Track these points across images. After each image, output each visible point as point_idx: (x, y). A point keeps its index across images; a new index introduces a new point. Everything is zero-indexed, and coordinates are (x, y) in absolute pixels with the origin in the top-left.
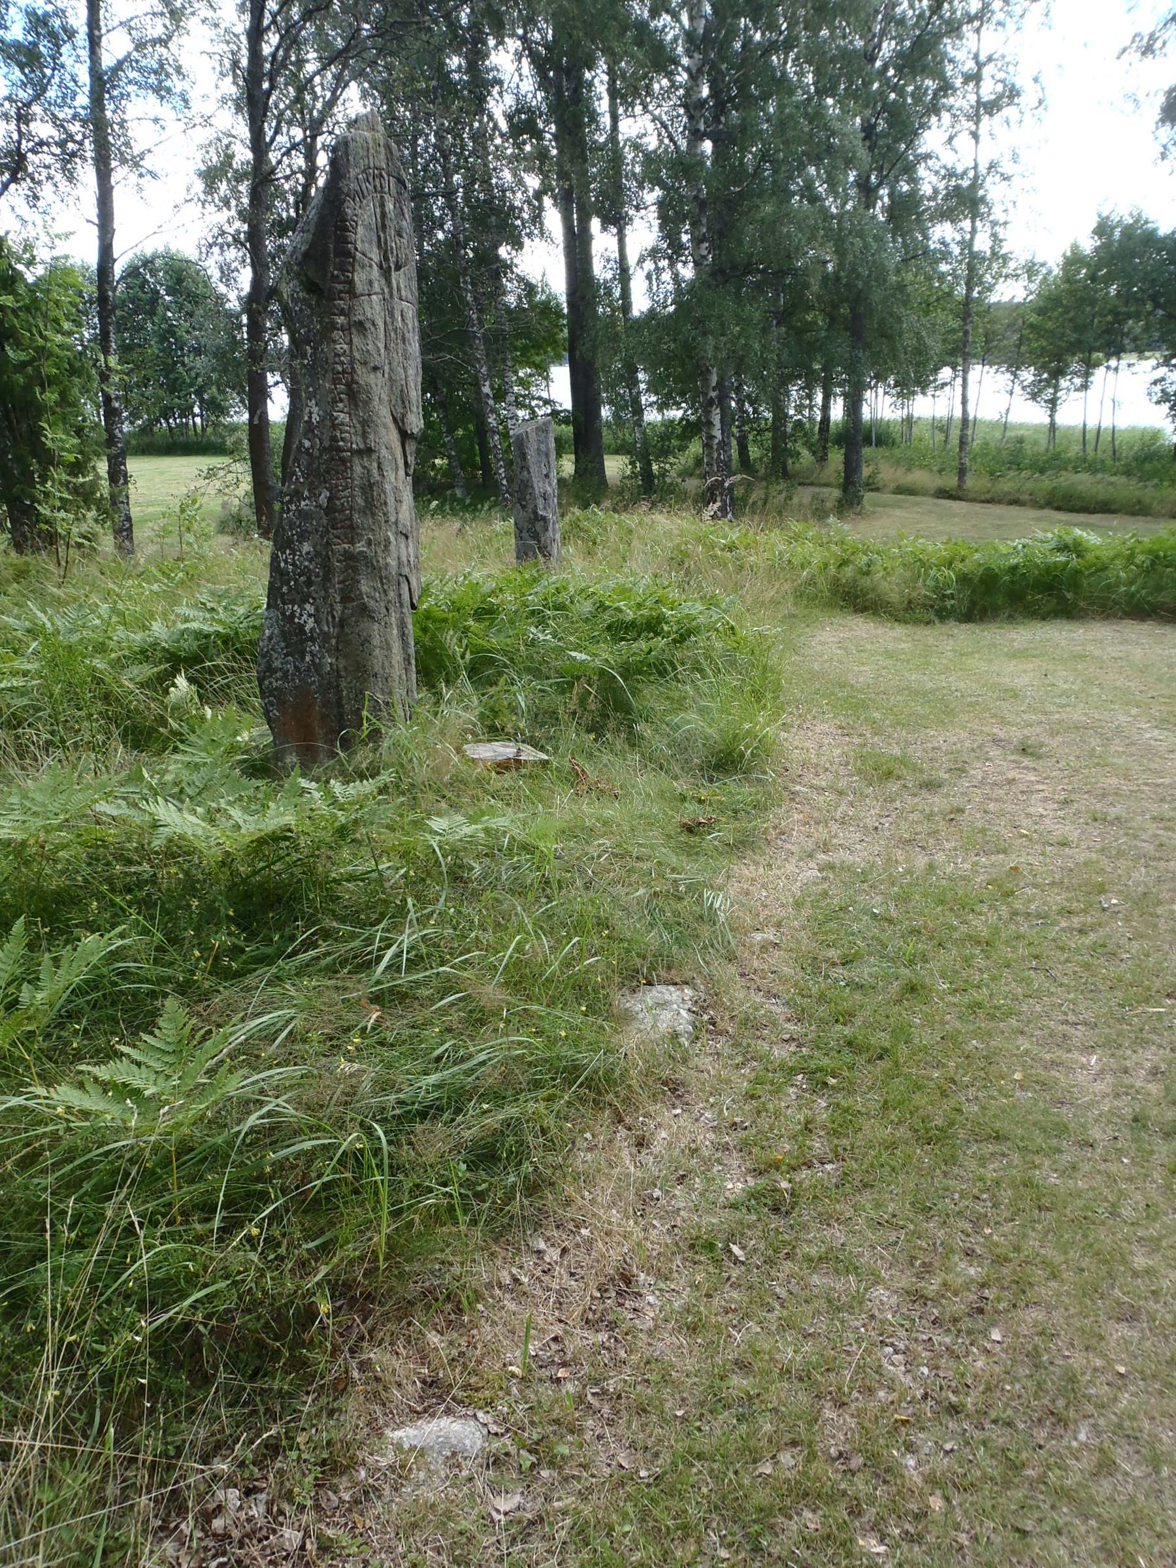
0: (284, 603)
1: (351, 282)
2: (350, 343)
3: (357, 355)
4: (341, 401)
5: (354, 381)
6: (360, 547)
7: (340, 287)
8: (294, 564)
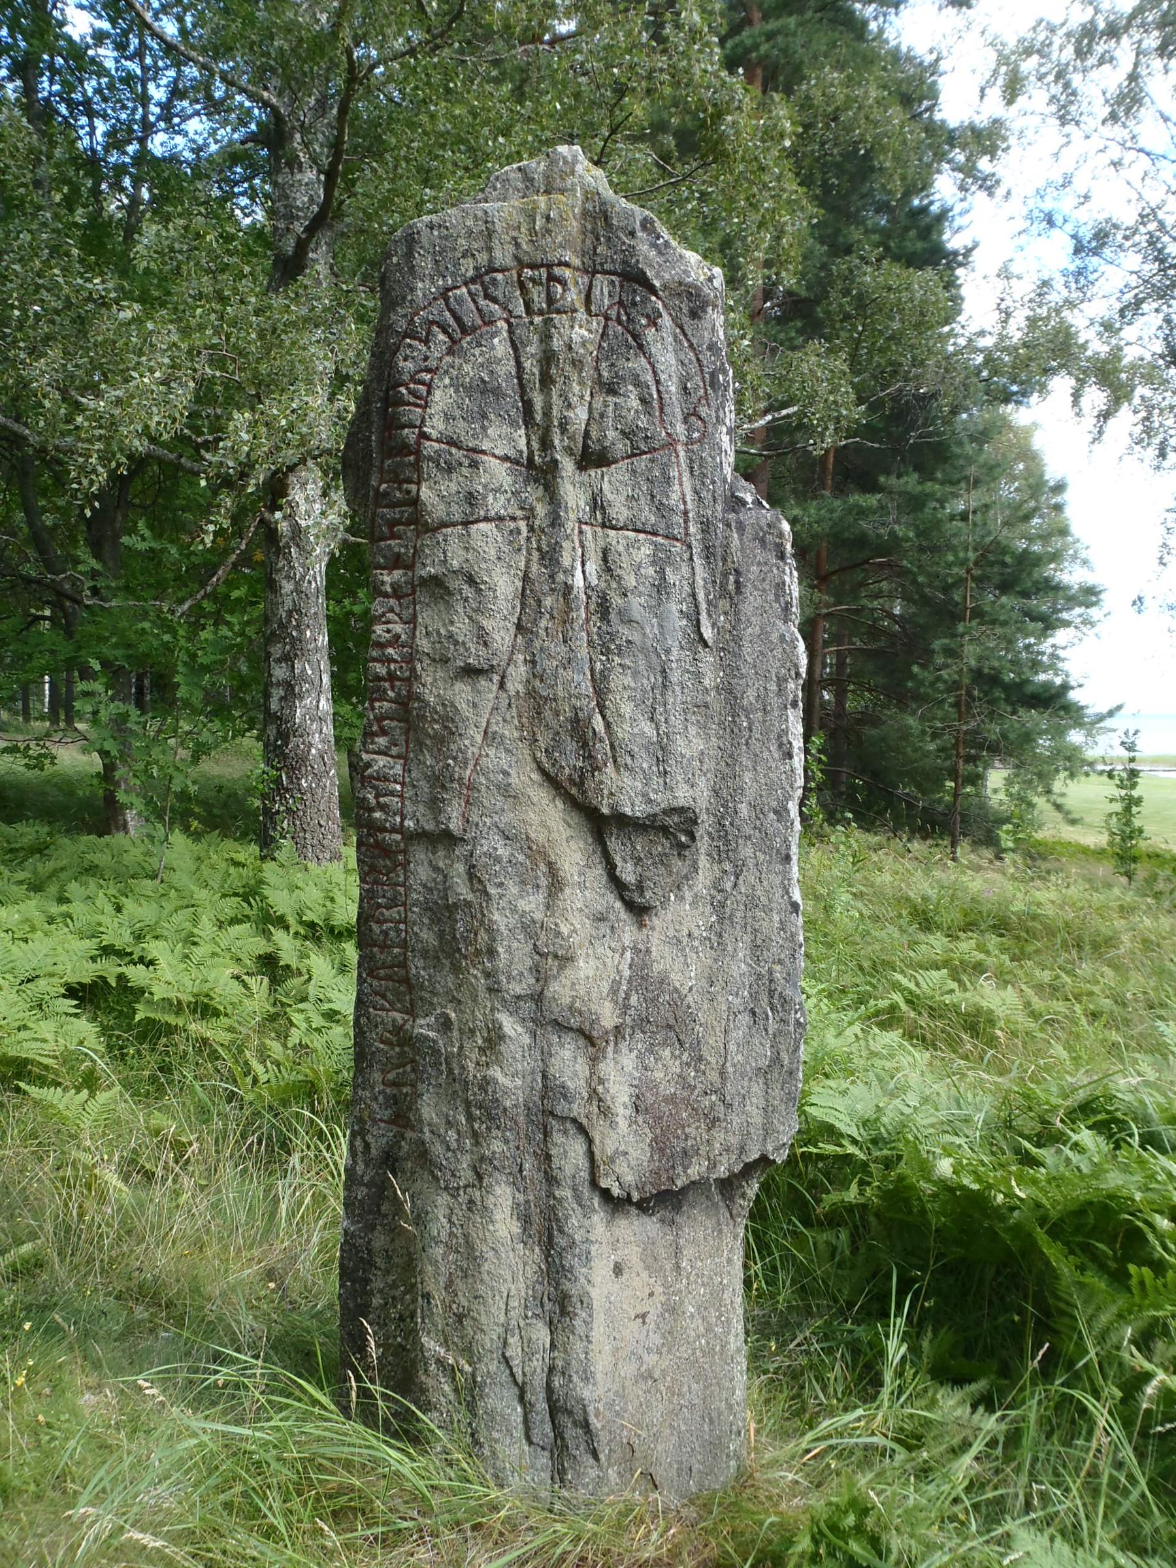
1: (415, 501)
2: (412, 621)
3: (424, 644)
4: (383, 732)
5: (412, 696)
6: (424, 1027)
7: (396, 513)
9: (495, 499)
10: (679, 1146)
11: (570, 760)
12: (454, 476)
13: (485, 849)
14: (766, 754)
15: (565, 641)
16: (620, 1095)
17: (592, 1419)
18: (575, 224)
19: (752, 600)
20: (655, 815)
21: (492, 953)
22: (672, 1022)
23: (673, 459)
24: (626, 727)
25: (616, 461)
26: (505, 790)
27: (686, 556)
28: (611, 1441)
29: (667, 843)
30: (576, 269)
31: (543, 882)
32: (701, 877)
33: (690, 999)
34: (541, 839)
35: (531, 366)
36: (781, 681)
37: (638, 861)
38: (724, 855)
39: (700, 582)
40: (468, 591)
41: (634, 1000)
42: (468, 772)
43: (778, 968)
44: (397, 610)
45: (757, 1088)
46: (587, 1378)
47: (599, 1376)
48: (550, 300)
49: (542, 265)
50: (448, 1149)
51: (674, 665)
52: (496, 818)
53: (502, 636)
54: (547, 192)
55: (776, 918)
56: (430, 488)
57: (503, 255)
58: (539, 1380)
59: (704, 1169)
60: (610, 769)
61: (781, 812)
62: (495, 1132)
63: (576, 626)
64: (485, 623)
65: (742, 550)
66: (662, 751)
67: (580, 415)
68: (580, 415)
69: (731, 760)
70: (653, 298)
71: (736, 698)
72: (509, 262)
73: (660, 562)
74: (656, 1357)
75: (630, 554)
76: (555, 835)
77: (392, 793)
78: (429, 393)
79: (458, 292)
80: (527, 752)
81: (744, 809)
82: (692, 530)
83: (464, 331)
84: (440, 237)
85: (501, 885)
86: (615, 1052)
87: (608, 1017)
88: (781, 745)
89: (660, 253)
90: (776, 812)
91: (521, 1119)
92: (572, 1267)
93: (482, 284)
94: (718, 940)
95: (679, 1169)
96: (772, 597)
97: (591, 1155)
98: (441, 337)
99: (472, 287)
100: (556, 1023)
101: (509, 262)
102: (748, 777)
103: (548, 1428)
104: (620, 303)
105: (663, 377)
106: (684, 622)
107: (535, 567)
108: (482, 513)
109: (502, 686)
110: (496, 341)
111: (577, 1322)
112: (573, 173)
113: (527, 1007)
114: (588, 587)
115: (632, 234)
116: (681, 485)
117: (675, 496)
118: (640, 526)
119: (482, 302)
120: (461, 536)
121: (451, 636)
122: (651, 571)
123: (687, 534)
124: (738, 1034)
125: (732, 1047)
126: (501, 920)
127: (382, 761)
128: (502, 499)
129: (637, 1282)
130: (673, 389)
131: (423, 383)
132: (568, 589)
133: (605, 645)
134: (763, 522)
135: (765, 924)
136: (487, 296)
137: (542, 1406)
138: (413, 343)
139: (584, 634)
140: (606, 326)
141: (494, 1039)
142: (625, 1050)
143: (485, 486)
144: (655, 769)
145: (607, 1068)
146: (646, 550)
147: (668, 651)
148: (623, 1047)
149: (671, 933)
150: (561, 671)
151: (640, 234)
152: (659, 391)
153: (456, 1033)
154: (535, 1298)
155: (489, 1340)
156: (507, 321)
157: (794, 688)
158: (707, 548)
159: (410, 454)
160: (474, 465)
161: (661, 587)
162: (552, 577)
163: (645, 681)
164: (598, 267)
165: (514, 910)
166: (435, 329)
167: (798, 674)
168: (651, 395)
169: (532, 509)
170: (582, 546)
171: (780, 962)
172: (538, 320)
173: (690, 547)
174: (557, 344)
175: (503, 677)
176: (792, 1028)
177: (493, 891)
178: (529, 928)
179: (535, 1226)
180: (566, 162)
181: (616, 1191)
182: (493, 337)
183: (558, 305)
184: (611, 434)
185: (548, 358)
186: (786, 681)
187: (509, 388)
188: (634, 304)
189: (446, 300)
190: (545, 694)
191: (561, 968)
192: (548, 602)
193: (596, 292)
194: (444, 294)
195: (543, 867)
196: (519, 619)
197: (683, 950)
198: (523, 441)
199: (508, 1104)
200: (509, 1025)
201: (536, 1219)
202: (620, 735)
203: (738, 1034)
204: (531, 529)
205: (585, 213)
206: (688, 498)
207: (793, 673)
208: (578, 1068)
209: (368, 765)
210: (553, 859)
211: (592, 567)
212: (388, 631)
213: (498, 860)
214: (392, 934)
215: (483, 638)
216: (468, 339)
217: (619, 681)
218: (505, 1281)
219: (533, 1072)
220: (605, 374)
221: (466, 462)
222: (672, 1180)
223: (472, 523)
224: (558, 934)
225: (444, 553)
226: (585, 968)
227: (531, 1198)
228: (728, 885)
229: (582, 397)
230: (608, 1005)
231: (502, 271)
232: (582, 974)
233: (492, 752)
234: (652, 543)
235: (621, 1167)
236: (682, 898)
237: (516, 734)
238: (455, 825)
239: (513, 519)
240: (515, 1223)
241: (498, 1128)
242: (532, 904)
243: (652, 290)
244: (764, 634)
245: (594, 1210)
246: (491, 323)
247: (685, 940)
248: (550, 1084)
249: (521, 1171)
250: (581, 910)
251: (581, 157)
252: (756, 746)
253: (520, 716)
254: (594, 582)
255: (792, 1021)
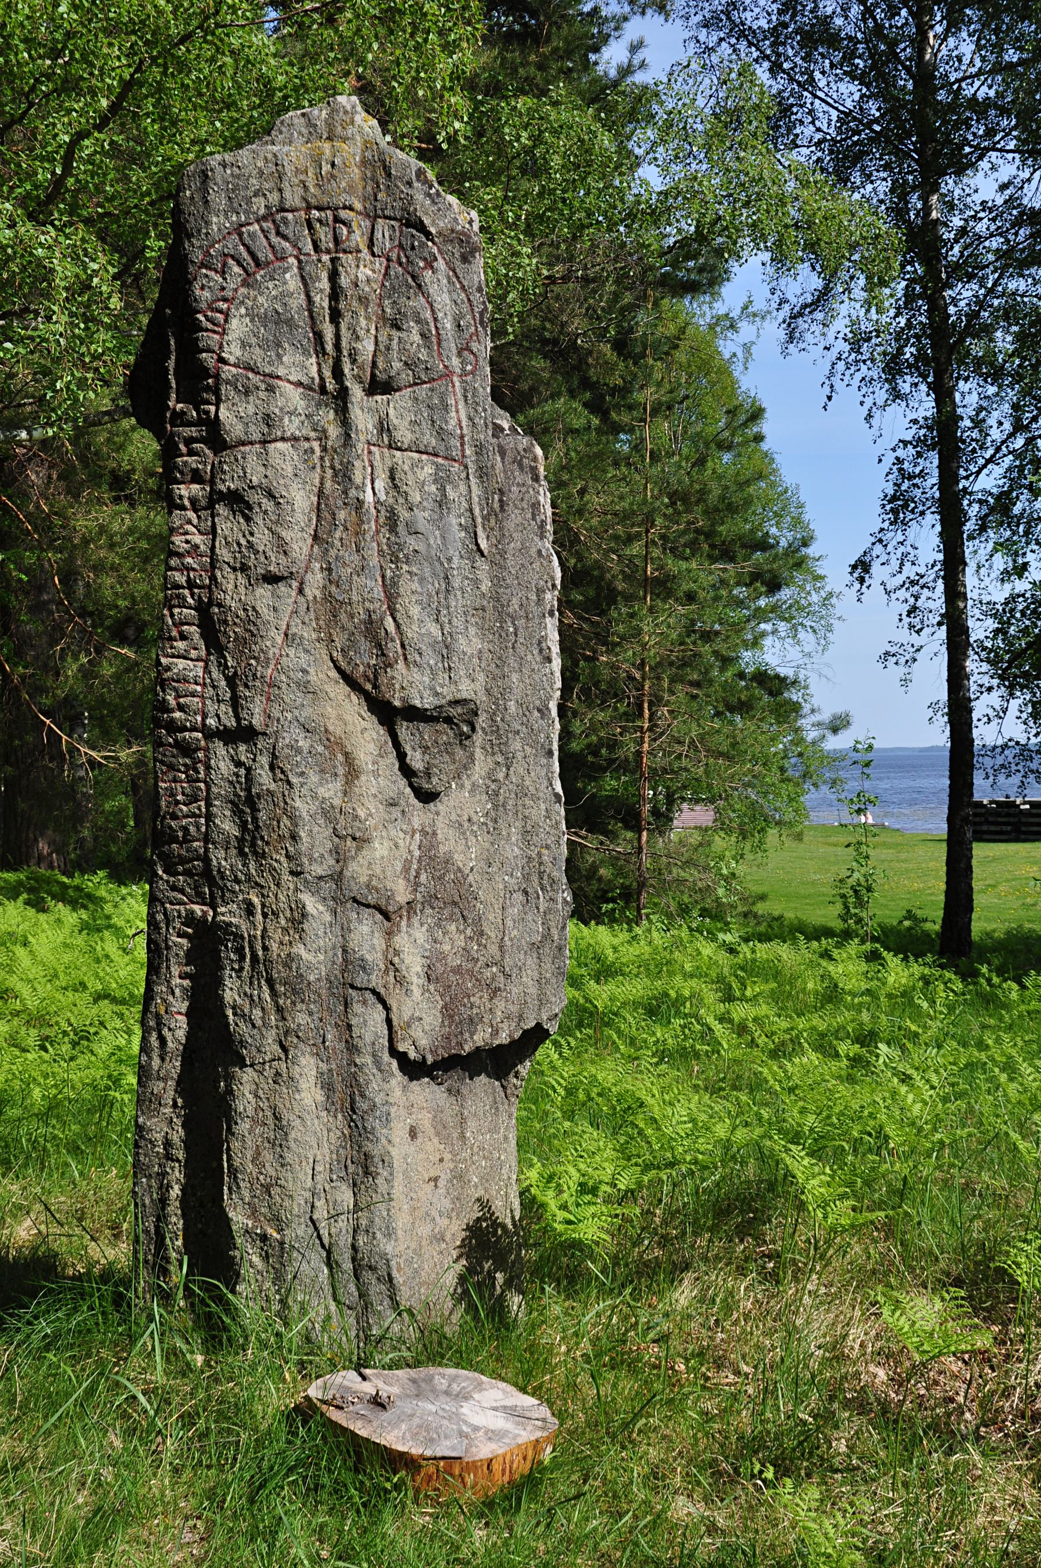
3: (224, 554)
4: (183, 637)
6: (229, 914)
9: (290, 421)
10: (466, 1013)
11: (364, 659)
12: (251, 399)
13: (287, 741)
14: (529, 657)
15: (358, 551)
16: (413, 965)
17: (395, 1273)
18: (356, 171)
19: (515, 518)
20: (441, 707)
21: (294, 837)
22: (457, 899)
23: (450, 389)
24: (415, 628)
25: (399, 389)
26: (305, 687)
27: (463, 475)
28: (411, 1296)
29: (451, 733)
30: (359, 213)
31: (341, 771)
32: (477, 768)
33: (471, 878)
34: (339, 732)
35: (322, 301)
36: (540, 592)
37: (426, 749)
38: (496, 749)
39: (475, 499)
40: (268, 504)
41: (423, 878)
42: (270, 671)
43: (545, 851)
44: (195, 521)
45: (531, 962)
46: (389, 1234)
47: (399, 1232)
48: (337, 240)
49: (329, 208)
50: (254, 1026)
51: (455, 572)
52: (296, 713)
53: (300, 545)
54: (329, 138)
55: (543, 807)
56: (228, 409)
57: (293, 197)
58: (345, 1241)
59: (488, 1036)
60: (401, 665)
61: (544, 711)
62: (299, 1006)
63: (368, 537)
64: (284, 534)
65: (505, 472)
66: (446, 650)
67: (367, 347)
68: (367, 347)
69: (501, 662)
70: (430, 244)
71: (503, 606)
72: (298, 203)
73: (442, 481)
74: (446, 1221)
75: (414, 473)
76: (350, 728)
77: (193, 694)
78: (226, 321)
79: (251, 228)
80: (324, 652)
81: (512, 704)
82: (468, 452)
83: (258, 264)
84: (232, 175)
85: (302, 774)
86: (408, 926)
87: (402, 894)
88: (541, 651)
89: (434, 202)
90: (539, 710)
91: (324, 992)
92: (373, 1128)
93: (274, 221)
94: (493, 825)
95: (467, 1035)
96: (529, 516)
97: (389, 1021)
98: (237, 269)
99: (264, 225)
100: (355, 900)
101: (298, 203)
102: (515, 677)
103: (352, 1288)
104: (401, 246)
105: (440, 315)
106: (463, 534)
107: (328, 484)
108: (279, 434)
109: (301, 591)
110: (288, 276)
111: (380, 1181)
112: (352, 122)
113: (328, 886)
114: (378, 502)
115: (409, 184)
116: (457, 411)
117: (453, 422)
118: (422, 448)
119: (275, 240)
120: (259, 455)
121: (251, 545)
122: (433, 488)
123: (463, 456)
124: (514, 911)
125: (509, 923)
126: (302, 806)
127: (181, 663)
128: (296, 421)
129: (429, 1147)
130: (448, 326)
131: (221, 312)
132: (360, 503)
133: (394, 555)
134: (520, 447)
135: (534, 812)
136: (278, 233)
137: (348, 1266)
138: (209, 273)
139: (375, 544)
140: (388, 268)
141: (299, 919)
142: (416, 924)
143: (281, 409)
144: (440, 665)
145: (401, 940)
146: (429, 470)
147: (450, 560)
148: (415, 921)
149: (454, 817)
150: (355, 577)
151: (416, 184)
152: (437, 328)
153: (259, 917)
154: (339, 1162)
155: (298, 1205)
156: (297, 258)
157: (551, 598)
158: (481, 468)
159: (211, 377)
160: (271, 389)
161: (442, 503)
162: (345, 492)
163: (430, 586)
164: (379, 212)
165: (314, 797)
166: (231, 261)
167: (554, 586)
168: (430, 331)
169: (324, 431)
170: (372, 466)
171: (548, 847)
172: (325, 258)
173: (466, 467)
174: (344, 281)
175: (301, 583)
176: (560, 906)
177: (294, 780)
178: (328, 813)
179: (337, 1094)
180: (346, 112)
181: (412, 1055)
182: (285, 272)
183: (344, 246)
184: (397, 365)
185: (335, 293)
186: (544, 591)
187: (302, 320)
188: (413, 248)
189: (240, 235)
190: (340, 598)
191: (359, 849)
192: (342, 515)
193: (378, 235)
194: (239, 227)
195: (340, 757)
196: (316, 531)
197: (464, 833)
198: (315, 368)
199: (312, 978)
200: (312, 904)
201: (338, 1087)
202: (409, 635)
203: (514, 911)
204: (324, 449)
205: (364, 162)
206: (464, 424)
207: (549, 584)
208: (375, 941)
209: (168, 669)
210: (349, 749)
211: (379, 485)
212: (187, 542)
213: (299, 751)
214: (192, 829)
215: (282, 547)
216: (262, 272)
217: (408, 586)
218: (311, 1147)
219: (334, 948)
220: (388, 310)
221: (263, 387)
222: (460, 1045)
223: (269, 442)
224: (356, 817)
225: (243, 469)
226: (380, 849)
227: (334, 1066)
228: (501, 776)
229: (368, 331)
230: (401, 882)
231: (292, 211)
232: (378, 855)
233: (292, 652)
234: (434, 463)
235: (417, 1032)
236: (462, 786)
237: (314, 636)
238: (258, 721)
239: (307, 439)
240: (319, 1092)
241: (303, 1001)
242: (331, 791)
243: (428, 234)
244: (523, 550)
245: (392, 1074)
246: (283, 259)
247: (466, 824)
248: (350, 957)
249: (324, 1042)
250: (375, 796)
251: (359, 108)
252: (521, 650)
253: (317, 619)
254: (383, 498)
255: (560, 900)
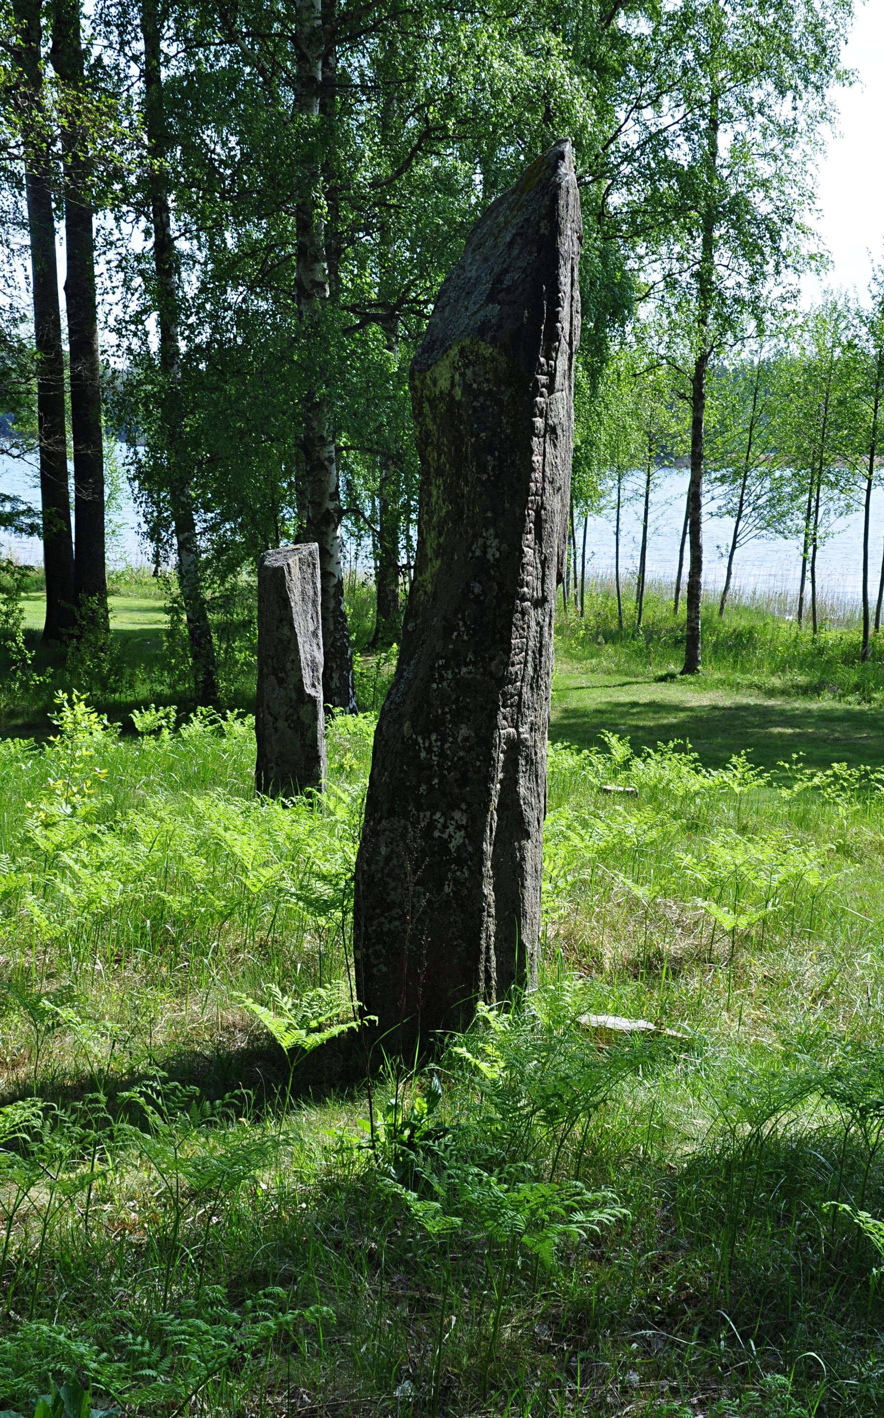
0: (419, 809)
8: (442, 755)
